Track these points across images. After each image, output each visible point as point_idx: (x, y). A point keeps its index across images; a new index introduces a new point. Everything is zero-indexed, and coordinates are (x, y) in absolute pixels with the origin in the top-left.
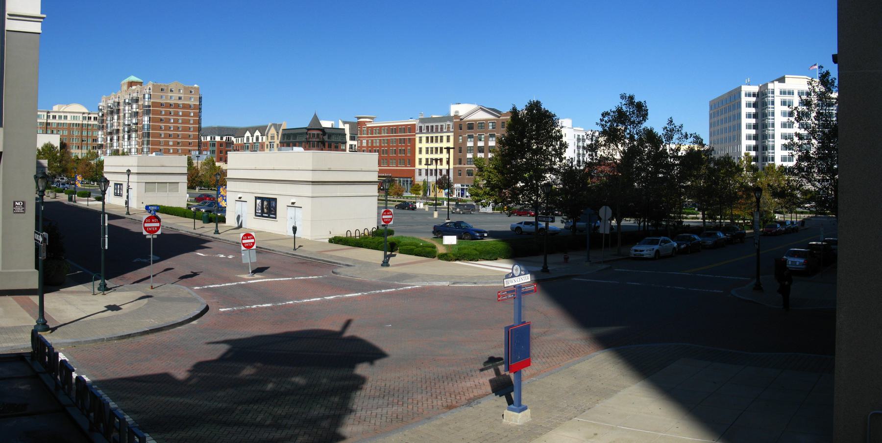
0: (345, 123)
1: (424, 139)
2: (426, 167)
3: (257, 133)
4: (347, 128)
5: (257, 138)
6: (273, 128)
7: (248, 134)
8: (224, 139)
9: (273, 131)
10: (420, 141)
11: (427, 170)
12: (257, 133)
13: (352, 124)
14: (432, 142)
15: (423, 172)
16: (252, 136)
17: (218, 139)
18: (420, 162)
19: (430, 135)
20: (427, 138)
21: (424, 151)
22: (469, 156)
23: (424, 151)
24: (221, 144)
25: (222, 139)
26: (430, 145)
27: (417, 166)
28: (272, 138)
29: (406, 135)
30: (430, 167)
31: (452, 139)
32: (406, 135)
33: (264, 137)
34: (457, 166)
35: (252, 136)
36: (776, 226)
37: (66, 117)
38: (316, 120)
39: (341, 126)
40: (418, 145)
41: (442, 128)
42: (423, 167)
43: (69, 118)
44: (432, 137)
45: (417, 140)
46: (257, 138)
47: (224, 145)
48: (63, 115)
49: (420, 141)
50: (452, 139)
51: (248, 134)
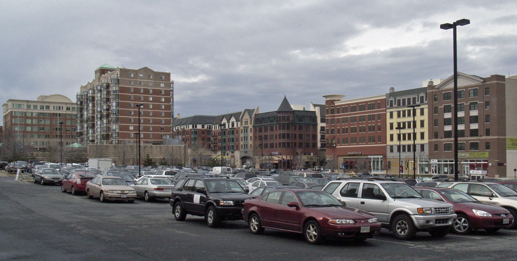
0: (315, 106)
1: (395, 114)
2: (398, 143)
3: (233, 119)
4: (317, 110)
5: (233, 125)
6: (246, 113)
7: (224, 121)
8: (206, 127)
9: (247, 117)
10: (391, 116)
11: (399, 147)
12: (233, 119)
13: (322, 107)
14: (404, 116)
15: (395, 149)
16: (228, 122)
17: (199, 127)
18: (392, 139)
19: (401, 109)
20: (399, 112)
21: (395, 137)
22: (448, 128)
23: (395, 137)
24: (203, 132)
25: (203, 127)
26: (402, 120)
27: (389, 143)
28: (246, 122)
29: (375, 112)
30: (403, 131)
31: (426, 111)
32: (375, 112)
33: (239, 123)
34: (434, 140)
35: (228, 122)
36: (191, 198)
37: (48, 107)
38: (285, 102)
39: (312, 109)
40: (389, 121)
41: (414, 102)
42: (396, 142)
43: (51, 108)
44: (404, 112)
45: (388, 115)
46: (233, 125)
47: (206, 133)
48: (45, 105)
49: (391, 116)
50: (426, 111)
51: (224, 121)
